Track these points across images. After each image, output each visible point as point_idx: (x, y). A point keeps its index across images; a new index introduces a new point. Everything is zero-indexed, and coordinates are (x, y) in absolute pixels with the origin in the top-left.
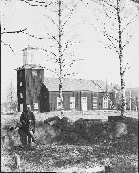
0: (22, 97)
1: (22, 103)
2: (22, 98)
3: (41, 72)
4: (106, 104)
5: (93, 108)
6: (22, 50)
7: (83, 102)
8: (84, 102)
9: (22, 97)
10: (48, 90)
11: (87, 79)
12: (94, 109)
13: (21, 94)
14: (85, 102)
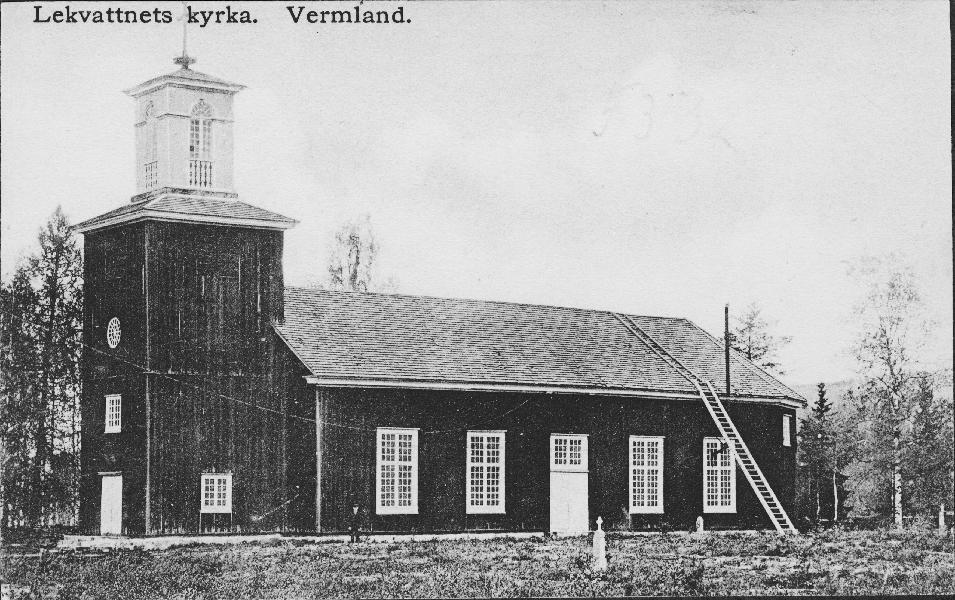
0: (113, 427)
1: (111, 468)
2: (117, 429)
3: (267, 242)
4: (388, 483)
5: (471, 510)
6: (127, 92)
7: (560, 467)
8: (568, 467)
9: (113, 427)
10: (310, 380)
11: (587, 308)
12: (208, 517)
13: (113, 403)
14: (574, 467)
